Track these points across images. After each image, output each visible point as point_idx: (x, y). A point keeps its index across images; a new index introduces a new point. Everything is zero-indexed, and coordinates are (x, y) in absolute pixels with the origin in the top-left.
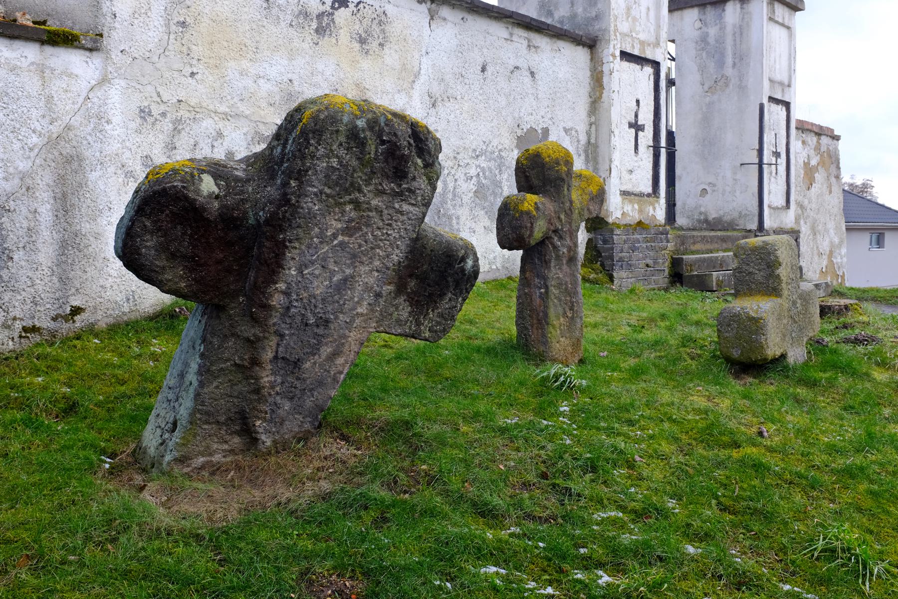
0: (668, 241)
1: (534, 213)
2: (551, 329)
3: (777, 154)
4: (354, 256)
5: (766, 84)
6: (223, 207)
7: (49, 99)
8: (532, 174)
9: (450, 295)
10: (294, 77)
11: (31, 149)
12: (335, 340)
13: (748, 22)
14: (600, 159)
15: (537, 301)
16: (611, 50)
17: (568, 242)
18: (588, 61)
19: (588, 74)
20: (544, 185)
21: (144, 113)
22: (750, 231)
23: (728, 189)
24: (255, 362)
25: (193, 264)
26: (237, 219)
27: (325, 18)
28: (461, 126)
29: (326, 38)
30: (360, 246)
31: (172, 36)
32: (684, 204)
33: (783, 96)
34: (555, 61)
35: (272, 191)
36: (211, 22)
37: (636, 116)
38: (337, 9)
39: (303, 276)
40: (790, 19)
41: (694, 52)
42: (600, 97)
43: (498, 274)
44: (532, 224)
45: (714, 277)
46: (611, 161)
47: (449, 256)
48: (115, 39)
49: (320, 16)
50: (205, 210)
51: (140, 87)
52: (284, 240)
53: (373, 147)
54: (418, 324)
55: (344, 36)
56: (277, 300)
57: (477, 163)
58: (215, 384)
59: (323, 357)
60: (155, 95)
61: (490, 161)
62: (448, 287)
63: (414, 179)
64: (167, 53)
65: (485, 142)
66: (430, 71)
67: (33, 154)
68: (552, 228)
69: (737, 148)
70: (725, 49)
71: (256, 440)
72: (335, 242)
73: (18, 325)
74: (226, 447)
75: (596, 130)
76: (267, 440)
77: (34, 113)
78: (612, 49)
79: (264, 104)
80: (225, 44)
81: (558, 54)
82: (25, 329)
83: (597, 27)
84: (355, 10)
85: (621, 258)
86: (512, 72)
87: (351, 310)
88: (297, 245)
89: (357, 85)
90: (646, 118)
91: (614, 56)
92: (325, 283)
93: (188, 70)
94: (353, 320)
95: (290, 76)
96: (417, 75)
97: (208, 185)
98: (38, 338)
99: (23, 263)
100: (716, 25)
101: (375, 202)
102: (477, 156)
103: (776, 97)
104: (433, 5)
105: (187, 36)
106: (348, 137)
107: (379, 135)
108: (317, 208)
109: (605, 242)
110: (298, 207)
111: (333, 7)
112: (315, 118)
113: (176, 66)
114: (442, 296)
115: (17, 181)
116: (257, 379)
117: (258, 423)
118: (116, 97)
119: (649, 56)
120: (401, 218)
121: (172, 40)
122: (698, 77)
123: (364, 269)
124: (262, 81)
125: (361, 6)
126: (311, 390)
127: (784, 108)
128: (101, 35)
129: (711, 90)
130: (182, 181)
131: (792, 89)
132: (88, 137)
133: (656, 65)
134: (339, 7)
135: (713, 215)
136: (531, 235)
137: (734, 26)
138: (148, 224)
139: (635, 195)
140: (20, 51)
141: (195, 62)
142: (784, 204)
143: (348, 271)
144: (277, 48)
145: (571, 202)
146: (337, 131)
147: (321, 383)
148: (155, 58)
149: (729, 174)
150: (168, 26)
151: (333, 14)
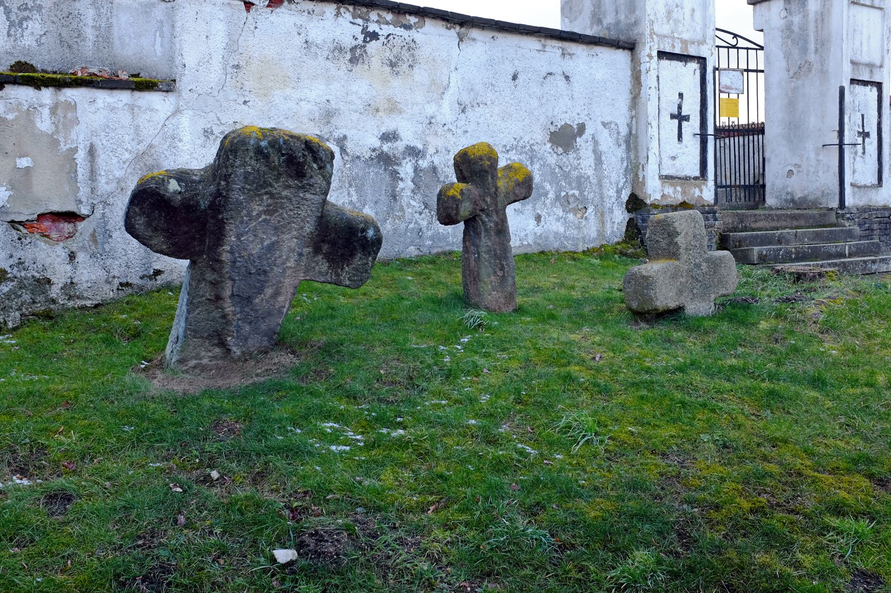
0: (716, 220)
1: (459, 197)
2: (483, 285)
3: (865, 135)
4: (276, 229)
7: (137, 128)
8: (463, 167)
9: (359, 255)
10: (330, 98)
11: (124, 163)
12: (274, 285)
13: (828, 9)
14: (640, 148)
15: (473, 263)
16: (647, 51)
17: (495, 218)
18: (629, 62)
19: (629, 73)
20: (472, 176)
22: (832, 209)
23: (812, 170)
24: (218, 298)
25: (170, 235)
26: (192, 206)
27: (358, 50)
28: (491, 126)
29: (359, 65)
31: (229, 76)
32: (773, 185)
34: (592, 64)
35: (212, 188)
37: (680, 107)
38: (368, 42)
39: (241, 241)
41: (780, 40)
42: (639, 93)
43: (529, 249)
45: (755, 253)
46: (648, 149)
47: (349, 228)
48: (184, 83)
49: (353, 49)
50: (171, 201)
52: (223, 218)
53: (276, 158)
54: (338, 275)
55: (375, 62)
56: (225, 257)
57: (508, 156)
58: (197, 312)
59: (268, 296)
61: (521, 154)
62: (355, 249)
63: (311, 177)
64: (225, 88)
65: (515, 139)
66: (460, 83)
67: (125, 166)
69: (820, 130)
70: (807, 35)
73: (116, 282)
74: (210, 354)
76: (237, 351)
77: (127, 138)
78: (648, 50)
79: (305, 120)
80: (272, 78)
81: (595, 59)
82: (121, 284)
83: (635, 32)
84: (385, 41)
88: (232, 221)
89: (389, 100)
90: (691, 107)
93: (241, 100)
94: (284, 271)
95: (327, 97)
97: (174, 185)
98: (130, 291)
99: (119, 239)
100: (800, 13)
101: (284, 193)
102: (508, 151)
104: (463, 29)
105: (241, 74)
106: (255, 153)
107: (280, 150)
109: (644, 221)
111: (364, 41)
112: (231, 142)
113: (231, 98)
114: (352, 255)
115: (114, 184)
116: (223, 308)
117: (229, 339)
119: (692, 51)
120: (307, 203)
122: (783, 64)
123: (286, 237)
124: (303, 103)
125: (391, 37)
126: (263, 318)
127: (875, 89)
128: (174, 81)
129: (796, 76)
131: (885, 70)
133: (702, 61)
134: (371, 40)
135: (798, 195)
137: (816, 13)
138: (137, 210)
139: (679, 178)
140: (117, 98)
141: (246, 93)
142: (876, 183)
143: (274, 239)
145: (497, 188)
146: (247, 150)
147: (270, 314)
149: (812, 156)
150: (225, 69)
151: (365, 46)
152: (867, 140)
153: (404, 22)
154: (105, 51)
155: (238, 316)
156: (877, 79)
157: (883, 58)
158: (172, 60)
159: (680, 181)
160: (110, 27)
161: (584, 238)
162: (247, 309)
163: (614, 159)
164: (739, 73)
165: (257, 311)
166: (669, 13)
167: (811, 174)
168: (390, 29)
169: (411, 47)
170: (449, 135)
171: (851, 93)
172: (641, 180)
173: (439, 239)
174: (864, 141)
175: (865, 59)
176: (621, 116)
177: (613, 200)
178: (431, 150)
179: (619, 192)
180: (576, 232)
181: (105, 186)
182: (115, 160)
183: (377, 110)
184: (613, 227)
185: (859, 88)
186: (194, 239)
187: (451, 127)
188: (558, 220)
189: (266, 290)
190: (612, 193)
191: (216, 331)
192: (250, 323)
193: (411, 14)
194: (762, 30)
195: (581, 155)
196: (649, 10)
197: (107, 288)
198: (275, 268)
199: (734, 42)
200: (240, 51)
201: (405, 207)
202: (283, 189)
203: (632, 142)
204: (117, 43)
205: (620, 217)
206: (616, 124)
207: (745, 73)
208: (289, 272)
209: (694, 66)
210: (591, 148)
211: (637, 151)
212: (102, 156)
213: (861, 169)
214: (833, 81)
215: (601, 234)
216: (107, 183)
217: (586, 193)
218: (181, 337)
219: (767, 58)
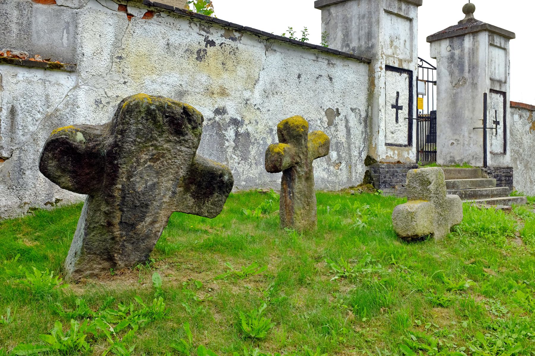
2: (295, 216)
3: (497, 123)
4: (157, 173)
5: (488, 82)
6: (87, 147)
7: (47, 96)
8: (284, 132)
9: (217, 194)
11: (37, 121)
12: (153, 215)
14: (373, 125)
15: (288, 200)
17: (305, 169)
21: (98, 102)
23: (466, 143)
24: (110, 224)
25: (74, 174)
30: (160, 168)
31: (114, 64)
33: (500, 89)
34: (345, 71)
36: (136, 56)
40: (505, 44)
44: (281, 159)
46: (379, 126)
48: (85, 64)
49: (199, 52)
50: (77, 148)
51: (96, 89)
53: (161, 119)
54: (200, 208)
58: (92, 234)
60: (103, 93)
62: (214, 189)
68: (295, 161)
69: (471, 118)
70: (464, 62)
71: (116, 263)
72: (146, 165)
73: (27, 207)
74: (100, 266)
75: (372, 109)
77: (39, 103)
78: (380, 64)
80: (144, 67)
85: (385, 181)
86: (317, 78)
87: (160, 200)
88: (125, 166)
90: (404, 101)
91: (381, 68)
92: (143, 186)
93: (122, 80)
95: (180, 82)
96: (257, 81)
97: (80, 137)
99: (30, 176)
100: (459, 48)
103: (495, 89)
105: (123, 63)
108: (133, 148)
110: (123, 148)
112: (128, 105)
113: (116, 79)
114: (212, 194)
116: (113, 232)
117: (116, 255)
118: (83, 95)
119: (405, 66)
121: (114, 66)
122: (449, 78)
125: (223, 45)
126: (143, 240)
127: (502, 96)
128: (76, 65)
129: (456, 86)
130: (66, 135)
131: (507, 84)
132: (67, 115)
133: (410, 73)
136: (280, 165)
137: (469, 49)
138: (50, 155)
141: (126, 76)
142: (502, 151)
143: (155, 180)
144: (173, 69)
146: (140, 111)
147: (147, 236)
148: (104, 75)
149: (466, 134)
150: (112, 59)
152: (498, 126)
153: (233, 36)
154: (26, 41)
155: (124, 238)
156: (503, 90)
157: (506, 78)
158: (74, 50)
159: (397, 147)
160: (30, 24)
161: (339, 182)
162: (131, 233)
163: (357, 132)
164: (423, 83)
165: (139, 234)
166: (392, 42)
167: (466, 145)
168: (223, 40)
169: (234, 51)
170: (258, 112)
171: (490, 97)
172: (374, 146)
173: (250, 181)
174: (496, 127)
175: (497, 77)
176: (361, 103)
177: (357, 158)
178: (247, 122)
179: (360, 153)
180: (334, 178)
181: (22, 137)
182: (30, 119)
183: (213, 94)
184: (356, 176)
185: (494, 95)
186: (93, 178)
187: (259, 107)
188: (324, 170)
189: (147, 219)
190: (356, 153)
191: (106, 249)
192: (133, 243)
193: (236, 31)
194: (435, 58)
195: (339, 128)
196: (381, 39)
197: (19, 211)
198: (155, 203)
199: (420, 64)
200: (123, 47)
201: (229, 159)
202: (165, 142)
203: (369, 122)
204: (35, 36)
205: (361, 169)
206: (359, 110)
207: (427, 83)
208: (164, 206)
209: (405, 75)
210: (344, 124)
211: (371, 128)
212: (21, 115)
213: (495, 144)
214: (480, 90)
215: (349, 179)
216: (23, 135)
217: (341, 153)
218: (79, 253)
219: (438, 74)
